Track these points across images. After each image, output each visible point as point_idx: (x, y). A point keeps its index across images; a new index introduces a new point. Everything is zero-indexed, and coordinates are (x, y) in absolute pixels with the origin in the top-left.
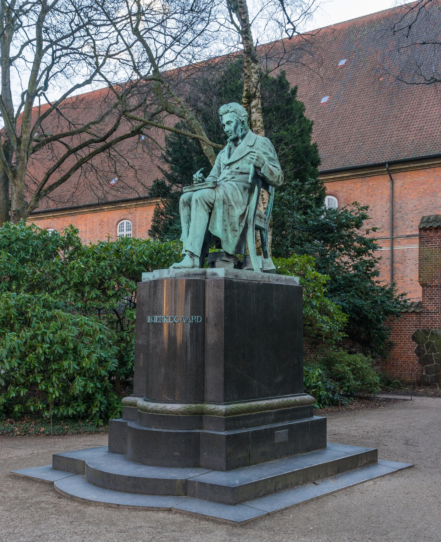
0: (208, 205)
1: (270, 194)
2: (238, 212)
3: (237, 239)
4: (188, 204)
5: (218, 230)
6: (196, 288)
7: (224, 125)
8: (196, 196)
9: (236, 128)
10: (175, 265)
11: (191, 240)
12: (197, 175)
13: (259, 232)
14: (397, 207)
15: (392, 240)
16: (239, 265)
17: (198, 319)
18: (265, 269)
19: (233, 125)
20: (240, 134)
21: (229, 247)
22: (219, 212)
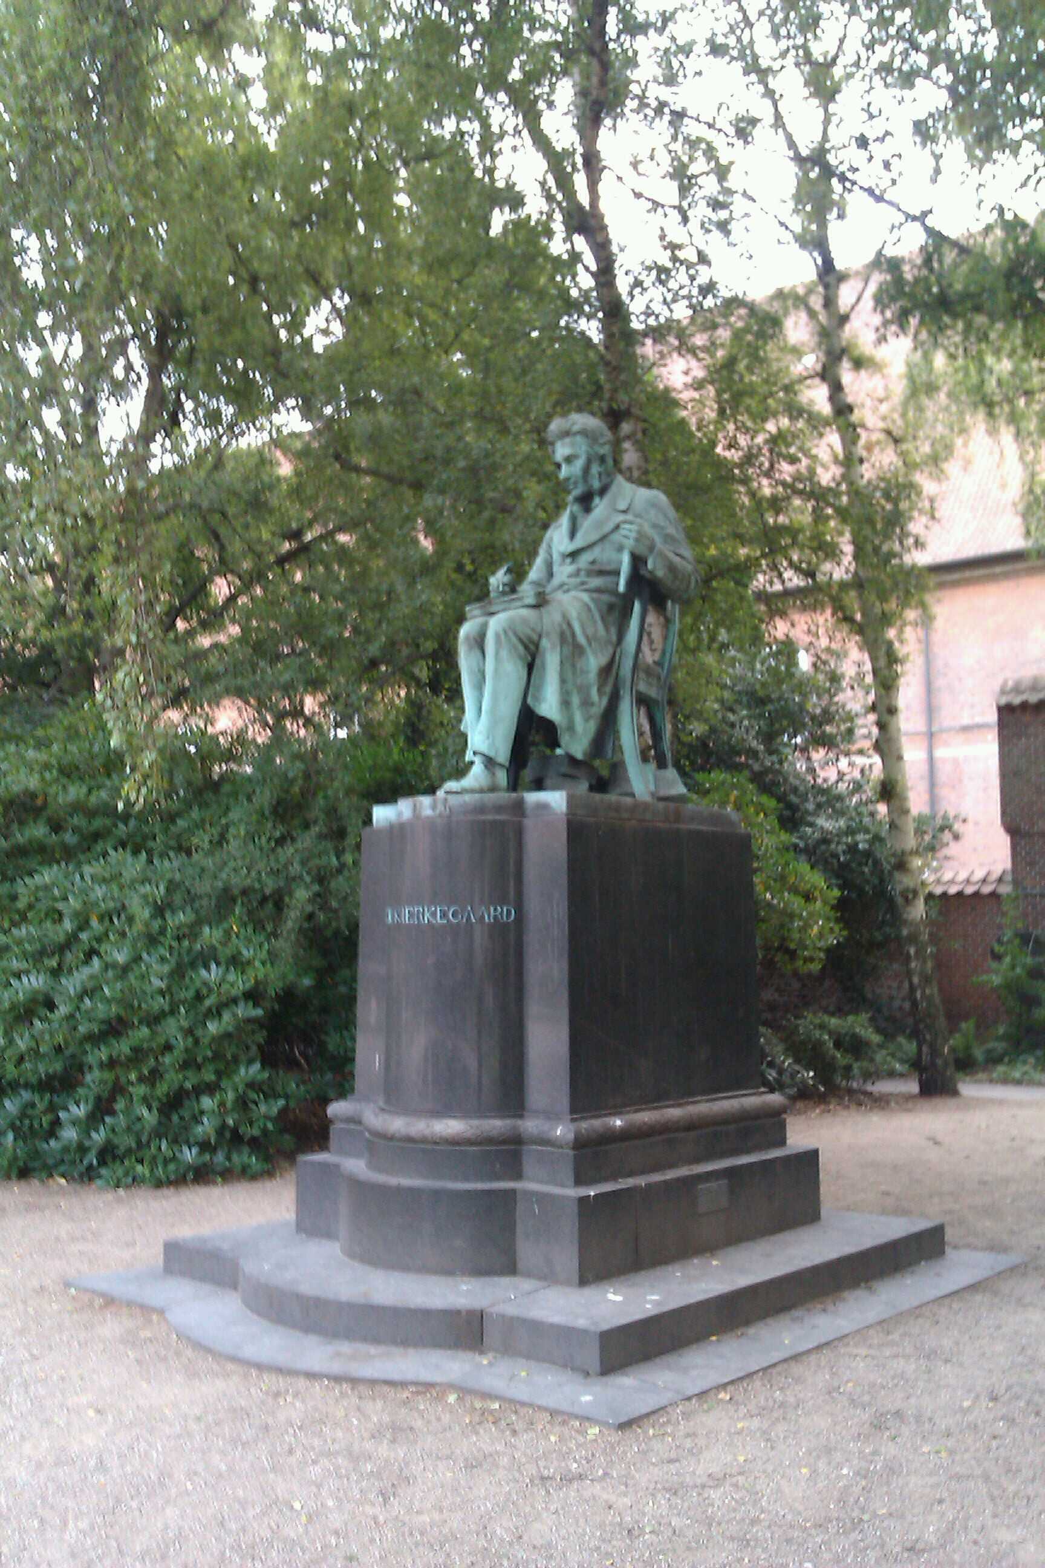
0: (526, 647)
1: (668, 621)
2: (594, 662)
3: (592, 726)
4: (479, 642)
5: (549, 707)
6: (498, 837)
7: (559, 466)
8: (495, 624)
9: (586, 470)
10: (451, 785)
11: (484, 726)
12: (498, 579)
13: (643, 710)
14: (939, 663)
15: (930, 737)
16: (601, 785)
17: (505, 913)
18: (663, 793)
19: (579, 464)
20: (596, 484)
21: (576, 743)
22: (552, 661)
